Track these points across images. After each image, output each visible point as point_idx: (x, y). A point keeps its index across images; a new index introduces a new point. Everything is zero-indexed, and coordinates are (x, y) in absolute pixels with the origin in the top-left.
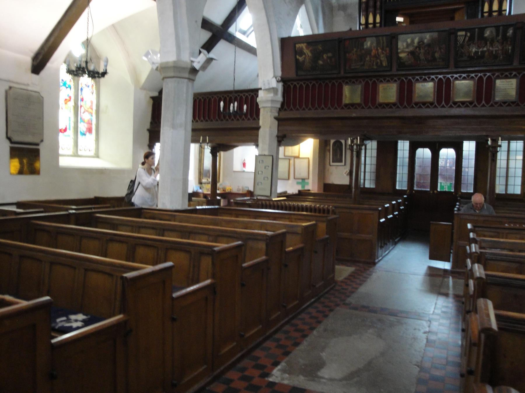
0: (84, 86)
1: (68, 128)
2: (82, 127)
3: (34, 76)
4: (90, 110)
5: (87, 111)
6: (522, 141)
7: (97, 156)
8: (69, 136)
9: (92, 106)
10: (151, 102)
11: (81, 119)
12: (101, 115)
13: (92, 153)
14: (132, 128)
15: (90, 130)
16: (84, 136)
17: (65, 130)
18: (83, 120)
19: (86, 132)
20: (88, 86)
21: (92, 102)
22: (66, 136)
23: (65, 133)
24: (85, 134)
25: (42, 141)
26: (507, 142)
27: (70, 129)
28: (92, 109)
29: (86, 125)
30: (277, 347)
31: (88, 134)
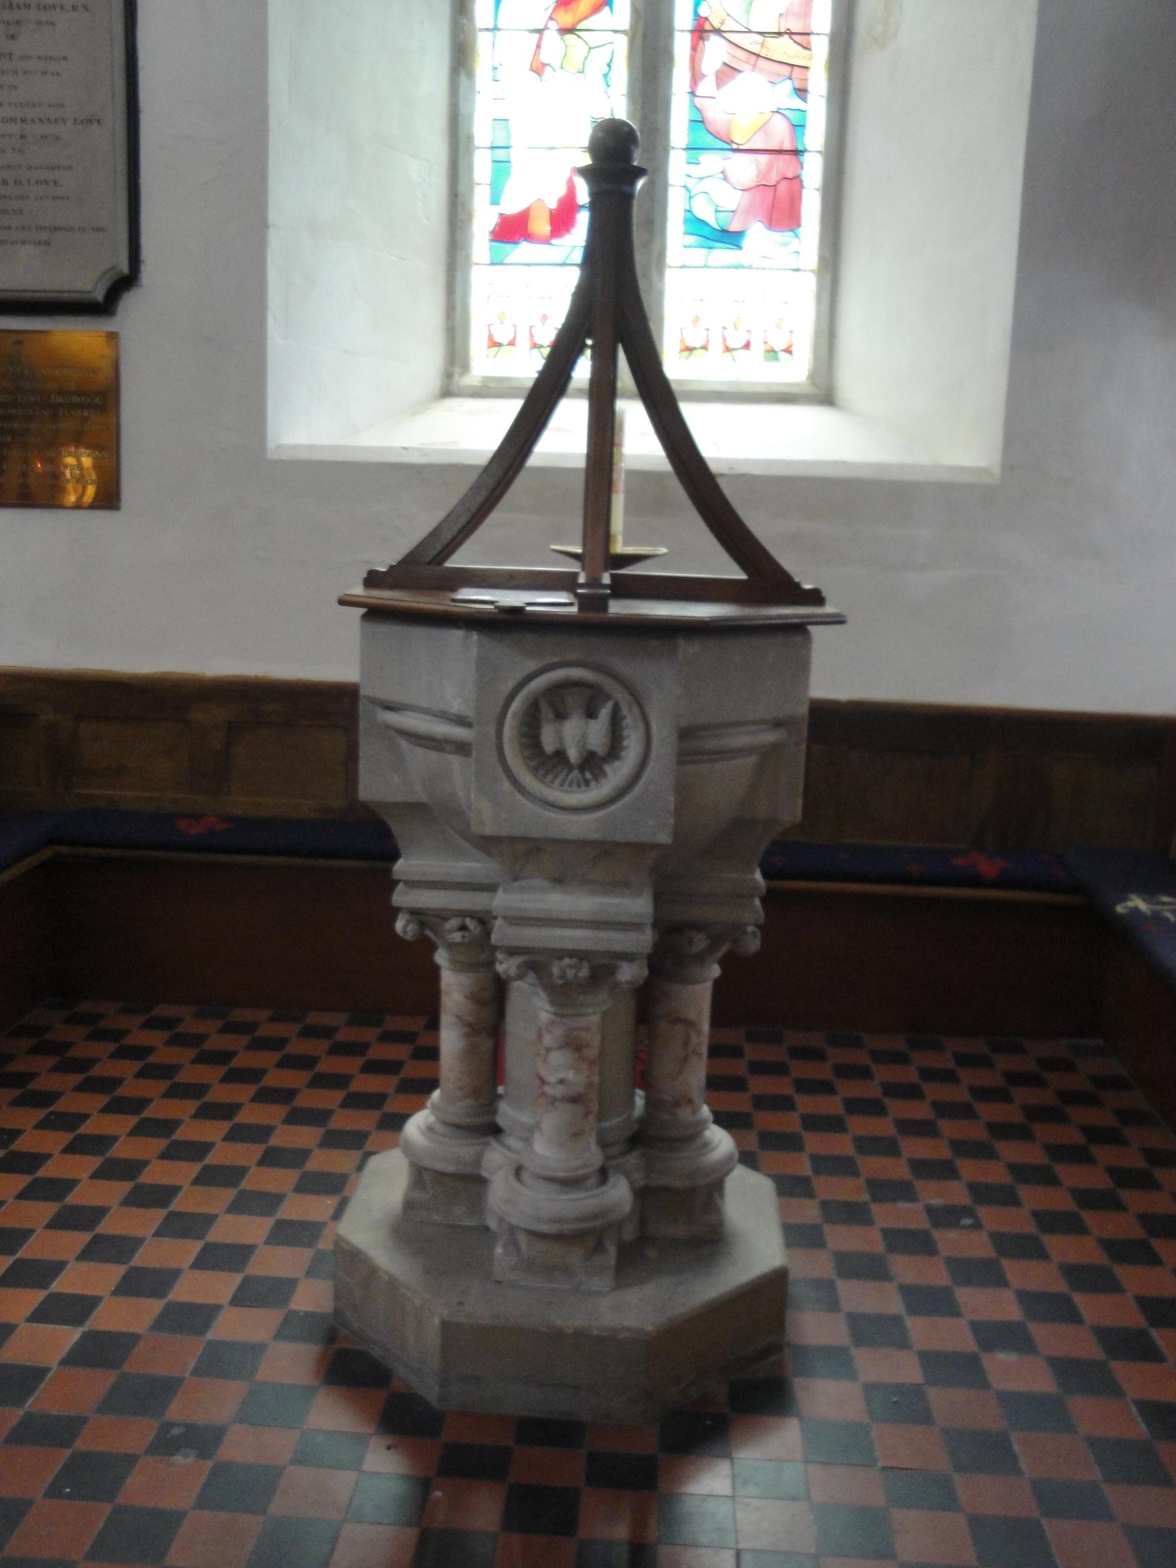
7: (823, 392)
11: (699, 122)
12: (870, 71)
13: (796, 371)
15: (781, 210)
16: (723, 254)
24: (730, 237)
29: (746, 169)
31: (758, 235)
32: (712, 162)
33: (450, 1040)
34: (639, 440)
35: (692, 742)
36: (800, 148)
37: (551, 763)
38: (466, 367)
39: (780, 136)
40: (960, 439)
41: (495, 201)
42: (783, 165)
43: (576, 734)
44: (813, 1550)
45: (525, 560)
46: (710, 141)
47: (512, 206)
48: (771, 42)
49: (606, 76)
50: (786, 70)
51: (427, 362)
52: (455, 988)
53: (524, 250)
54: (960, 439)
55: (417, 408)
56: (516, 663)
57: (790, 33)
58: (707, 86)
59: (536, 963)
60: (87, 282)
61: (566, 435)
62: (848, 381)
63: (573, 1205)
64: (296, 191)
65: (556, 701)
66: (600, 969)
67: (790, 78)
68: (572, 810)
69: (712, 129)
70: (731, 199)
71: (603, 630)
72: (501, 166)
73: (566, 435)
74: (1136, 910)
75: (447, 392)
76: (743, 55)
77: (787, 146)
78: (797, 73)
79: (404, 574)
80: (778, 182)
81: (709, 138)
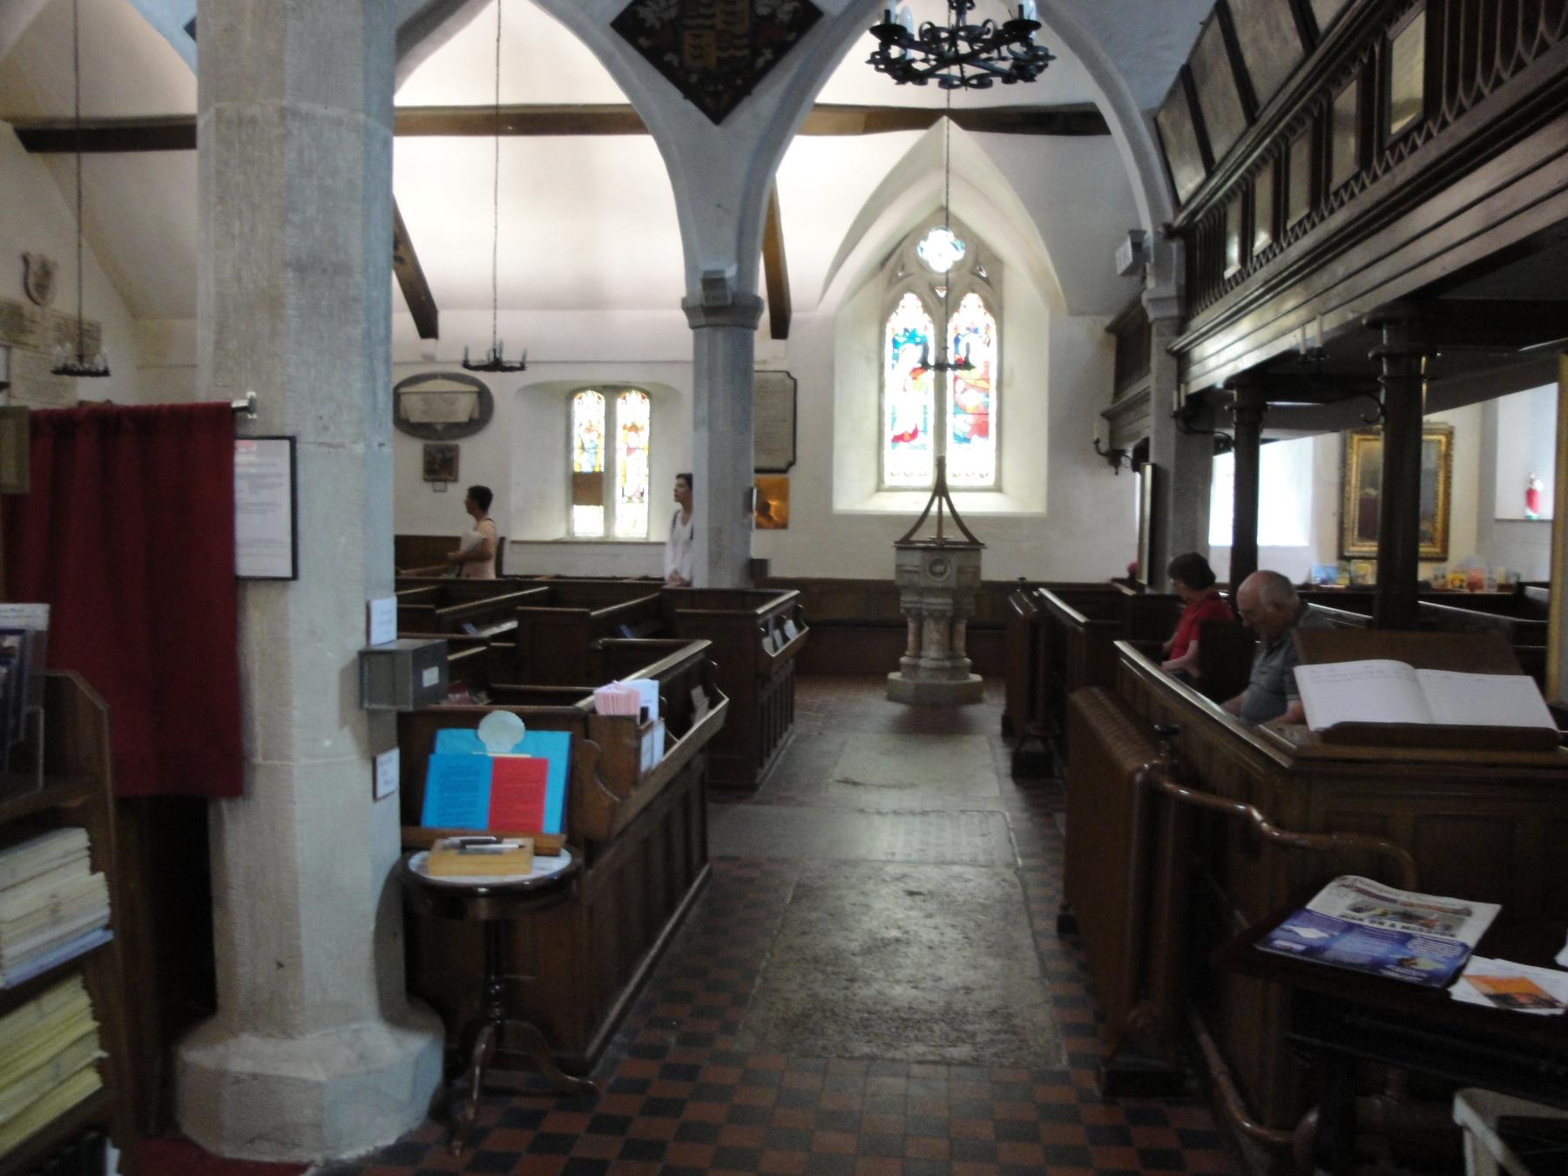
0: (962, 331)
1: (920, 428)
2: (957, 424)
3: (780, 343)
4: (982, 384)
5: (973, 387)
6: (76, 840)
7: (998, 488)
8: (924, 447)
9: (987, 372)
10: (1113, 338)
11: (956, 405)
12: (1007, 392)
13: (990, 481)
14: (1045, 412)
15: (982, 430)
16: (965, 445)
17: (914, 435)
18: (960, 408)
19: (972, 433)
20: (976, 331)
21: (987, 365)
22: (915, 447)
23: (914, 442)
24: (967, 440)
25: (792, 464)
26: (406, 149)
27: (925, 431)
28: (987, 380)
29: (971, 419)
30: (592, 1129)
31: (975, 438)
32: (961, 417)
33: (911, 638)
34: (946, 509)
35: (960, 571)
37: (934, 574)
39: (982, 410)
40: (1035, 505)
42: (982, 418)
43: (939, 568)
45: (927, 534)
47: (898, 433)
51: (871, 481)
52: (911, 626)
53: (902, 444)
54: (1035, 505)
55: (870, 497)
56: (929, 557)
59: (931, 614)
60: (781, 464)
61: (934, 509)
62: (1007, 483)
63: (940, 663)
64: (842, 436)
65: (935, 563)
66: (943, 614)
68: (938, 582)
70: (967, 429)
71: (941, 548)
72: (894, 420)
73: (934, 509)
74: (1250, 818)
79: (901, 541)
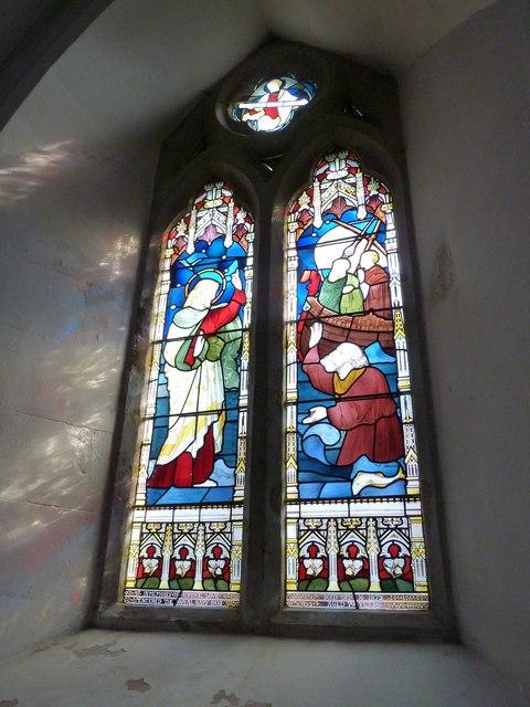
11: (306, 381)
12: (439, 322)
15: (386, 450)
36: (393, 390)
38: (113, 598)
41: (154, 456)
42: (381, 407)
44: (220, 408)
46: (316, 394)
48: (359, 320)
49: (236, 360)
50: (374, 336)
57: (373, 311)
58: (312, 356)
67: (378, 341)
69: (317, 384)
75: (90, 623)
76: (338, 331)
77: (381, 390)
78: (382, 337)
80: (377, 421)
81: (316, 393)
